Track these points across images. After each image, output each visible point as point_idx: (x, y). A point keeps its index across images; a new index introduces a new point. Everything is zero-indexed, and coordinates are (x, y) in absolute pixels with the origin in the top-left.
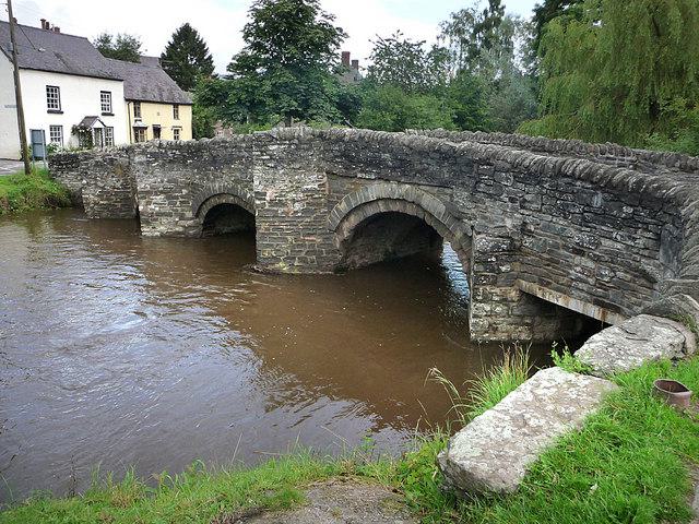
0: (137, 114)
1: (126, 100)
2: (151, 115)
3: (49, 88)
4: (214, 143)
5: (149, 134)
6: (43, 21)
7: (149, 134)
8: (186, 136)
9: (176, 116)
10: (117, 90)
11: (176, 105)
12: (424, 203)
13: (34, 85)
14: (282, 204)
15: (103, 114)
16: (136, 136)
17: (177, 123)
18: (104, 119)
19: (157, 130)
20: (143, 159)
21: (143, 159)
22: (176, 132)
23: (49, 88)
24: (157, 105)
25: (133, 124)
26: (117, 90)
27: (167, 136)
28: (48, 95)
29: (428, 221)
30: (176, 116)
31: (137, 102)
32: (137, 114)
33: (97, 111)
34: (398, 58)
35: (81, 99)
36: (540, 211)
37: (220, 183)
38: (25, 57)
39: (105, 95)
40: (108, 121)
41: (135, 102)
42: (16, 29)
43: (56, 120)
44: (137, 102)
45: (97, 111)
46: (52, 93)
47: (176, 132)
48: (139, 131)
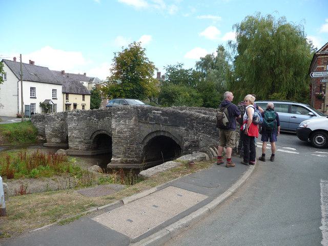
0: (67, 99)
1: (63, 93)
2: (74, 99)
3: (53, 90)
4: (98, 111)
5: (72, 107)
6: (30, 61)
7: (72, 107)
8: (88, 108)
9: (84, 100)
10: (59, 89)
11: (84, 95)
12: (170, 131)
13: (27, 86)
14: (121, 133)
15: (53, 99)
16: (66, 108)
17: (84, 102)
18: (53, 101)
19: (75, 105)
20: (71, 116)
21: (71, 116)
22: (83, 106)
23: (53, 90)
24: (76, 95)
25: (65, 103)
26: (59, 89)
27: (79, 108)
28: (31, 91)
29: (173, 139)
30: (84, 100)
31: (67, 94)
32: (67, 99)
33: (50, 97)
34: (178, 77)
35: (44, 92)
36: (203, 133)
37: (100, 125)
38: (24, 78)
39: (54, 91)
40: (55, 102)
41: (66, 94)
42: (23, 65)
43: (33, 101)
44: (67, 94)
45: (50, 97)
46: (32, 89)
47: (83, 106)
48: (68, 106)
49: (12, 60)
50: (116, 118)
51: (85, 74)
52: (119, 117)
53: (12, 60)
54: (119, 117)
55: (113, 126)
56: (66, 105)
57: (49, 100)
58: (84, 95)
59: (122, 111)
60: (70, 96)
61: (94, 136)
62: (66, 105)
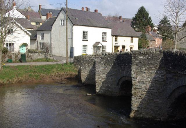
8: (136, 48)
9: (132, 41)
10: (109, 31)
11: (132, 37)
13: (78, 30)
15: (103, 41)
16: (115, 50)
17: (132, 44)
19: (123, 47)
22: (131, 48)
25: (114, 45)
26: (109, 31)
28: (103, 35)
30: (132, 41)
31: (116, 36)
32: (116, 40)
33: (100, 39)
39: (104, 34)
40: (104, 44)
41: (115, 36)
44: (116, 36)
46: (85, 33)
47: (131, 48)
48: (116, 47)
49: (81, 9)
50: (137, 64)
51: (96, 11)
52: (140, 63)
53: (81, 9)
54: (140, 63)
55: (133, 74)
56: (115, 46)
57: (99, 42)
58: (132, 37)
59: (145, 56)
60: (118, 38)
61: (121, 82)
62: (115, 46)
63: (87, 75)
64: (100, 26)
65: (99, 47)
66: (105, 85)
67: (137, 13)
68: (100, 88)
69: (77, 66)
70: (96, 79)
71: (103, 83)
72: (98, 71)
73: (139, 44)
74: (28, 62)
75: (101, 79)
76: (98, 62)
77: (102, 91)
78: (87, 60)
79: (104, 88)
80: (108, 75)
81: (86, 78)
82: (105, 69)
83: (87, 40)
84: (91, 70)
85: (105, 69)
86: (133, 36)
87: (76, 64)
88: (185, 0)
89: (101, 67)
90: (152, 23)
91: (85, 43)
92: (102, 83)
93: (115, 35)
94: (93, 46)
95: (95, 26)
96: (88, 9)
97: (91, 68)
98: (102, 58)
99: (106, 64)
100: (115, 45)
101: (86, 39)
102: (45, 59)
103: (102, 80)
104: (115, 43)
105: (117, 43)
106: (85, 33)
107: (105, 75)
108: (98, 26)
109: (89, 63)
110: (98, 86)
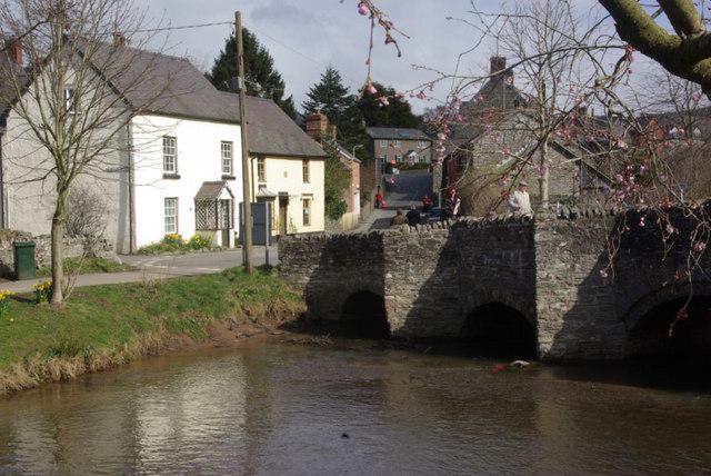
9: (306, 179)
17: (307, 188)
30: (306, 179)
41: (257, 155)
60: (269, 162)
63: (414, 303)
64: (214, 115)
65: (222, 201)
66: (575, 324)
67: (223, 56)
68: (557, 337)
69: (293, 276)
70: (540, 307)
71: (567, 316)
72: (548, 278)
73: (326, 185)
74: (116, 271)
75: (557, 305)
76: (545, 244)
77: (563, 346)
78: (409, 247)
79: (570, 337)
80: (586, 289)
81: (408, 316)
82: (573, 267)
83: (177, 177)
84: (428, 281)
85: (573, 267)
86: (308, 153)
87: (287, 270)
88: (708, 3)
89: (557, 261)
90: (289, 100)
91: (171, 188)
92: (564, 319)
93: (258, 150)
94: (196, 202)
95: (200, 114)
96: (122, 40)
97: (429, 276)
98: (560, 230)
99: (577, 250)
100: (261, 194)
101: (173, 172)
102: (89, 262)
103: (565, 309)
104: (260, 186)
105: (265, 186)
106: (169, 141)
107: (574, 290)
108: (207, 114)
109: (419, 256)
110: (547, 328)
